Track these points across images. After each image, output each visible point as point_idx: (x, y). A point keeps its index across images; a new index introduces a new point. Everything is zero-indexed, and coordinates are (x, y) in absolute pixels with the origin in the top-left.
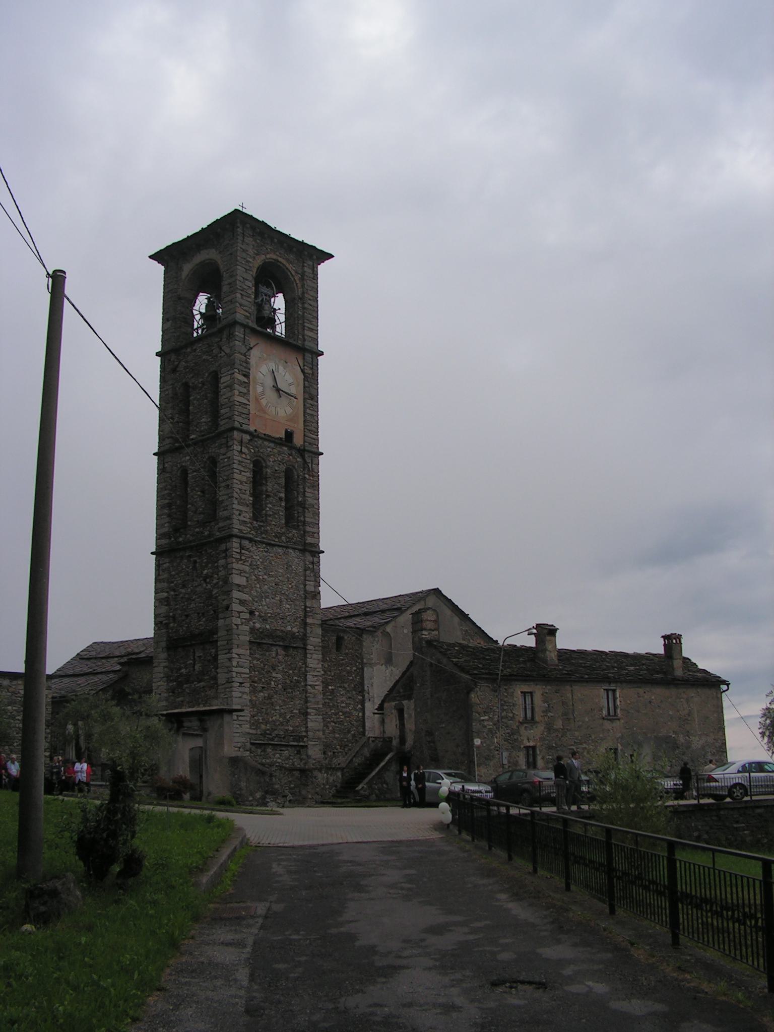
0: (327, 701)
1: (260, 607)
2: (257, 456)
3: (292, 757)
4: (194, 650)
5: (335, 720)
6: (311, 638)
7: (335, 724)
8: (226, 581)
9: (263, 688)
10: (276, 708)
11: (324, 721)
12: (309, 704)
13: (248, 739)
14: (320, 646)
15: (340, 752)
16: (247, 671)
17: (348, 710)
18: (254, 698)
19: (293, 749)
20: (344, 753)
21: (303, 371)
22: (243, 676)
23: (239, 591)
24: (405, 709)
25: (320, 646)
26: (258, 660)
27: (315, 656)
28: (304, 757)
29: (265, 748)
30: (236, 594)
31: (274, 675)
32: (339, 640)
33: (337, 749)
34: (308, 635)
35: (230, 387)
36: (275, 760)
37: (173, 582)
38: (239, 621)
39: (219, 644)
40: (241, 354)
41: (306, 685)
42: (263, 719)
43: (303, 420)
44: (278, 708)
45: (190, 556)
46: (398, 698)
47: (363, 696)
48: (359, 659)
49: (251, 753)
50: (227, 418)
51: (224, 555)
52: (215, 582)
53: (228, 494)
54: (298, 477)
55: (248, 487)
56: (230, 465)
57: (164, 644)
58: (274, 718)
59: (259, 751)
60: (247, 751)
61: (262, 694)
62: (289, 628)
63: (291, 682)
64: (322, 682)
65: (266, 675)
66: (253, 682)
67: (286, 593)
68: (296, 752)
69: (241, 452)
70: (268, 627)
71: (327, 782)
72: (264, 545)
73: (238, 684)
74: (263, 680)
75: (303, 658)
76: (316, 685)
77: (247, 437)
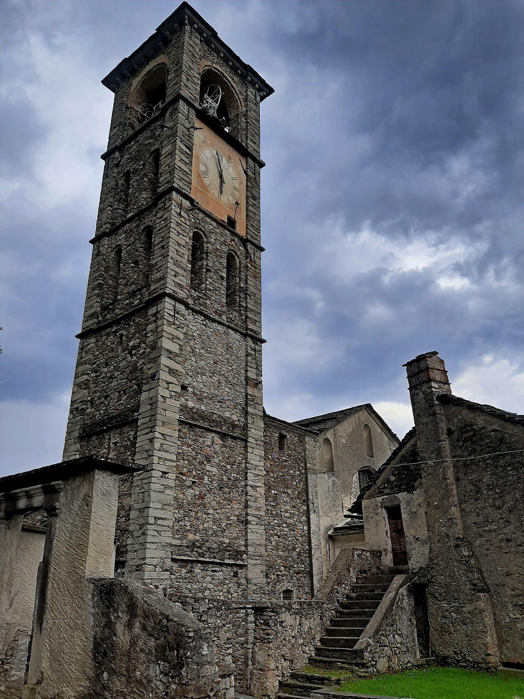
0: (269, 508)
1: (195, 383)
2: (197, 228)
3: (227, 582)
4: (110, 436)
5: (279, 534)
6: (253, 430)
7: (279, 537)
8: (154, 347)
9: (194, 483)
10: (209, 512)
11: (266, 533)
12: (249, 510)
13: (169, 553)
14: (262, 441)
15: (285, 575)
16: (174, 458)
17: (292, 521)
18: (181, 495)
19: (229, 568)
20: (289, 578)
21: (245, 172)
22: (168, 463)
23: (169, 358)
24: (403, 506)
25: (262, 441)
26: (189, 446)
27: (256, 451)
28: (243, 581)
29: (192, 567)
30: (164, 360)
31: (208, 468)
32: (282, 437)
33: (281, 571)
34: (249, 425)
35: (172, 154)
36: (204, 585)
37: (95, 363)
38: (167, 394)
39: (139, 423)
40: (185, 127)
41: (246, 485)
42: (191, 526)
43: (245, 215)
44: (211, 511)
45: (116, 332)
46: (387, 491)
47: (308, 506)
48: (302, 462)
49: (171, 574)
50: (166, 183)
51: (154, 318)
52: (142, 351)
53: (163, 255)
54: (240, 265)
55: (187, 254)
56: (166, 225)
57: (76, 434)
58: (206, 525)
59: (184, 571)
60: (166, 570)
61: (192, 491)
62: (227, 414)
63: (229, 479)
64: (264, 483)
65: (198, 467)
66: (179, 473)
67: (226, 374)
68: (232, 574)
69: (180, 214)
70: (203, 408)
71: (300, 632)
72: (203, 318)
73: (161, 474)
74: (194, 473)
75: (244, 452)
76: (258, 487)
77: (186, 204)
